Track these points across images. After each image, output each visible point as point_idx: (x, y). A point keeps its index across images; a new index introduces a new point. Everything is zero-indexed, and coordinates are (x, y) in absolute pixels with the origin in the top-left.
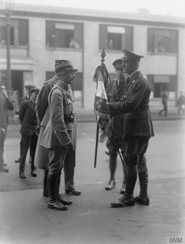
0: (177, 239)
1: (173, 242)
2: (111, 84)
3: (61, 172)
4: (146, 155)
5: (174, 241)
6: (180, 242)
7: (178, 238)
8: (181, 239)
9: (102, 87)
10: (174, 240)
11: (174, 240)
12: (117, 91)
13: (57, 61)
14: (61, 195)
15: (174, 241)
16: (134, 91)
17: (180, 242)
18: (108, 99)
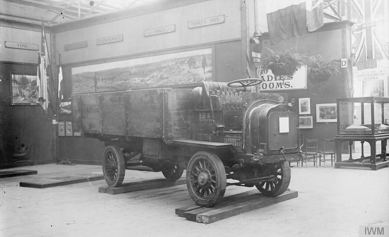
1: (369, 234)
5: (372, 232)
6: (380, 234)
7: (378, 228)
8: (383, 228)
10: (372, 231)
11: (372, 231)
15: (372, 232)
17: (380, 234)
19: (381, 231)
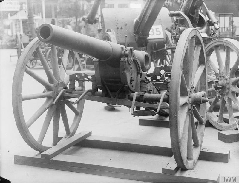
0: (231, 178)
1: (227, 181)
2: (33, 153)
3: (150, 28)
4: (227, 135)
5: (228, 180)
6: (234, 181)
7: (232, 178)
8: (235, 178)
9: (138, 24)
10: (228, 179)
11: (228, 179)
12: (29, 22)
13: (113, 5)
14: (148, 42)
15: (228, 180)
16: (181, 5)
17: (234, 181)
18: (193, 117)
19: (234, 179)
